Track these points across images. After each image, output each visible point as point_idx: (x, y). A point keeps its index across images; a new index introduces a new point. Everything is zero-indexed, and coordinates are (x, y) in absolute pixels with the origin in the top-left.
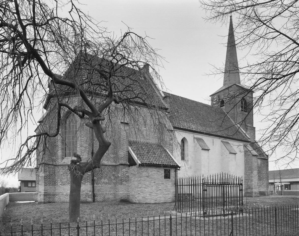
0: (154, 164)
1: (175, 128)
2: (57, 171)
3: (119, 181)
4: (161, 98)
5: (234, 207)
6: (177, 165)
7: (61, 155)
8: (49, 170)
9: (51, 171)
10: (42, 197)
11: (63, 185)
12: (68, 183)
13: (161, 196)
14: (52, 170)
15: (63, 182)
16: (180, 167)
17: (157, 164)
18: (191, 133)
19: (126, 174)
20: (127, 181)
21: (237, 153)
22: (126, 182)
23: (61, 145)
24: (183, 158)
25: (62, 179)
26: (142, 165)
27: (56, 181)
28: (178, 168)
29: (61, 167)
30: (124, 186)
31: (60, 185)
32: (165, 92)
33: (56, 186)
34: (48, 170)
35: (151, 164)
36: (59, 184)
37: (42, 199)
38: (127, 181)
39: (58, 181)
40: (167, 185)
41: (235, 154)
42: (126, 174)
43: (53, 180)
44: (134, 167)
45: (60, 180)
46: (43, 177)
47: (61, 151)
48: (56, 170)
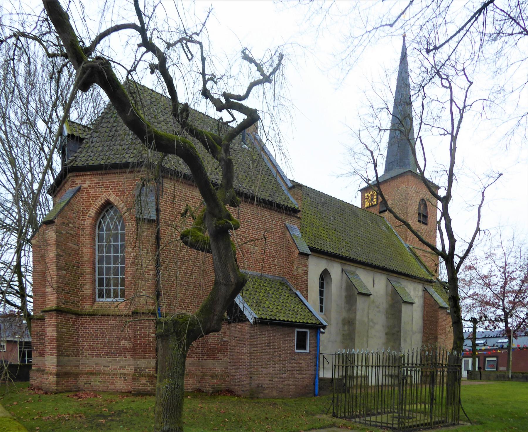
0: (280, 320)
1: (312, 249)
2: (82, 326)
3: (208, 351)
4: (284, 188)
5: (404, 407)
6: (319, 324)
7: (90, 294)
8: (67, 324)
9: (71, 327)
10: (52, 379)
11: (95, 355)
12: (105, 353)
13: (290, 382)
14: (72, 325)
15: (96, 350)
16: (324, 327)
17: (264, 319)
18: (324, 257)
19: (224, 337)
20: (225, 351)
21: (372, 293)
22: (223, 353)
23: (91, 274)
24: (321, 310)
25: (94, 344)
26: (261, 322)
27: (80, 348)
28: (322, 330)
29: (90, 318)
30: (218, 362)
31: (89, 354)
32: (293, 181)
33: (79, 356)
34: (65, 324)
35: (275, 320)
36: (86, 353)
37: (53, 384)
38: (225, 351)
39: (85, 347)
40: (301, 362)
41: (412, 304)
42: (223, 339)
43: (74, 345)
44: (239, 326)
45: (88, 346)
46: (54, 339)
47: (91, 285)
48: (81, 324)
